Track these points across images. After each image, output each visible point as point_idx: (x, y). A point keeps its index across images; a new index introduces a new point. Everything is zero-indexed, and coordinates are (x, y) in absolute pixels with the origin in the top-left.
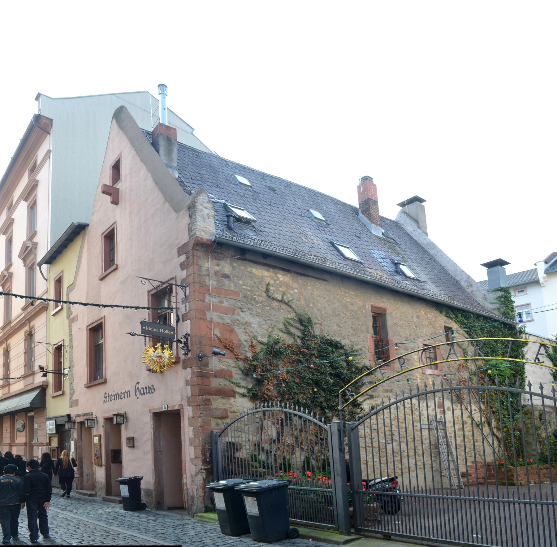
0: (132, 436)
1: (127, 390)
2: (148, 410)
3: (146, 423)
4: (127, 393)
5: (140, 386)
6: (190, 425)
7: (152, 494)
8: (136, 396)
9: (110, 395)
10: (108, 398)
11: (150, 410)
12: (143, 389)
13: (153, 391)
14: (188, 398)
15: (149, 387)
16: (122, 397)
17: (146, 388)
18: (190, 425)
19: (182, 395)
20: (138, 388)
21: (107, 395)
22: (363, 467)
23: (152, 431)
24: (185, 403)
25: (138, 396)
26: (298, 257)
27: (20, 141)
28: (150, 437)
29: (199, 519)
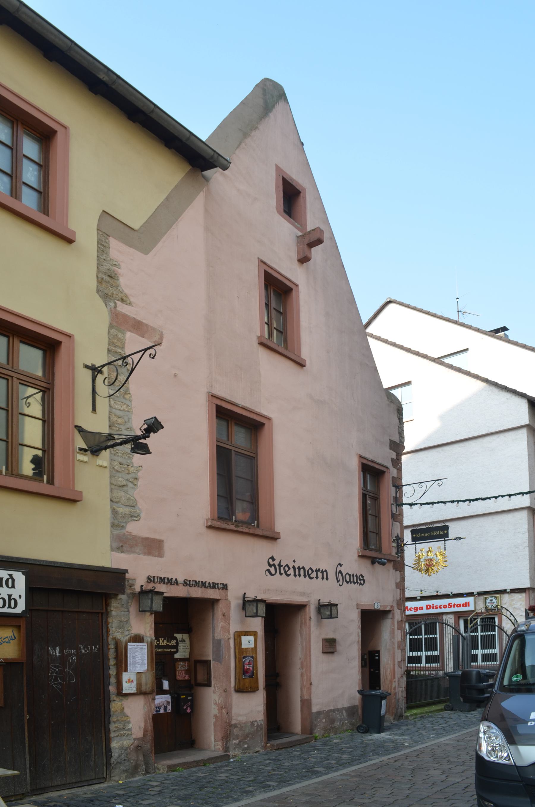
0: (330, 636)
1: (322, 568)
2: (355, 604)
3: (352, 621)
4: (322, 572)
5: (342, 569)
6: (398, 629)
7: (357, 711)
8: (338, 581)
9: (283, 564)
10: (274, 567)
11: (358, 605)
12: (350, 575)
13: (362, 582)
14: (398, 601)
15: (356, 576)
16: (314, 575)
17: (353, 575)
18: (398, 629)
19: (394, 596)
20: (340, 572)
21: (276, 563)
22: (452, 656)
23: (360, 631)
24: (395, 606)
25: (341, 583)
26: (445, 519)
27: (469, 370)
28: (357, 639)
29: (414, 717)
